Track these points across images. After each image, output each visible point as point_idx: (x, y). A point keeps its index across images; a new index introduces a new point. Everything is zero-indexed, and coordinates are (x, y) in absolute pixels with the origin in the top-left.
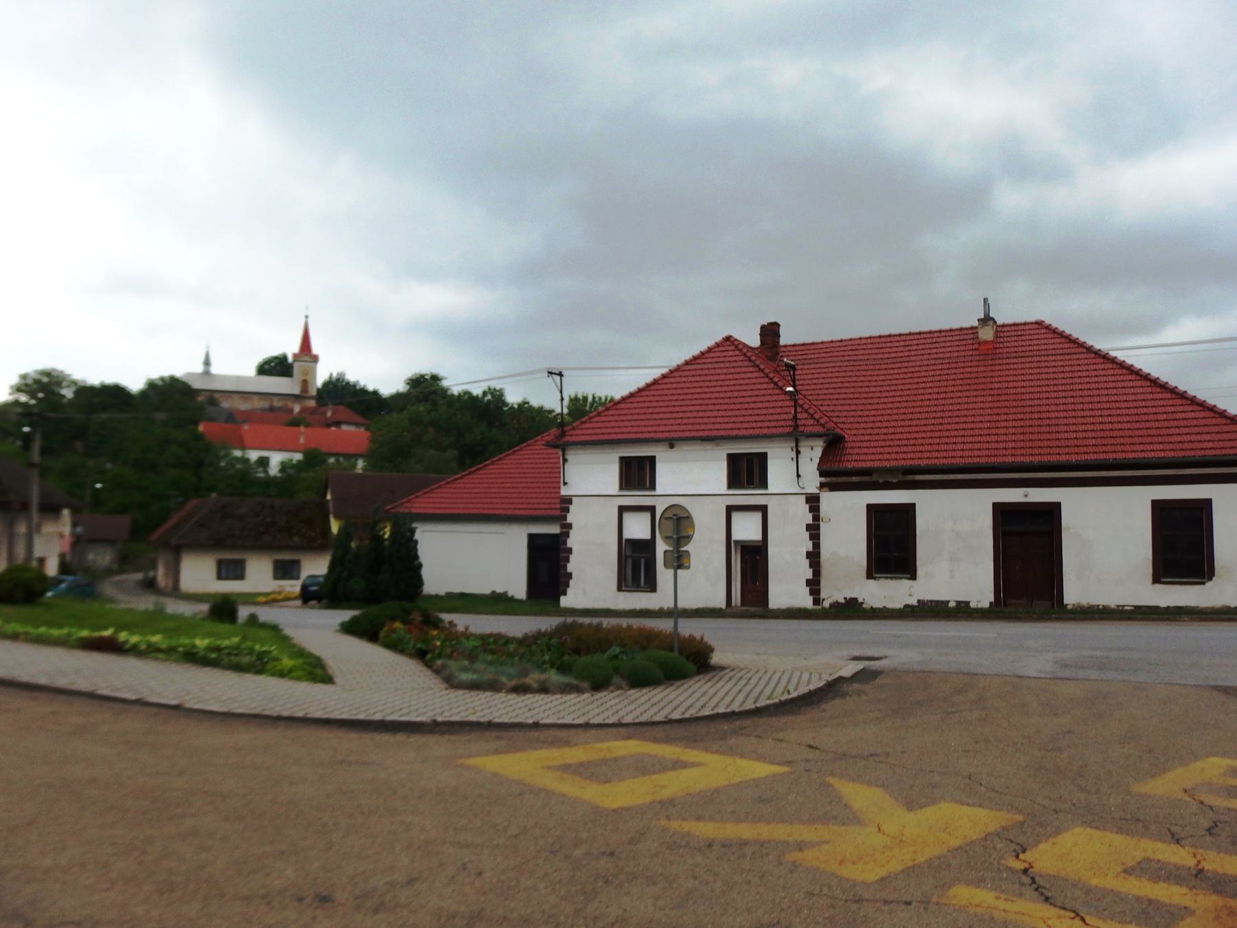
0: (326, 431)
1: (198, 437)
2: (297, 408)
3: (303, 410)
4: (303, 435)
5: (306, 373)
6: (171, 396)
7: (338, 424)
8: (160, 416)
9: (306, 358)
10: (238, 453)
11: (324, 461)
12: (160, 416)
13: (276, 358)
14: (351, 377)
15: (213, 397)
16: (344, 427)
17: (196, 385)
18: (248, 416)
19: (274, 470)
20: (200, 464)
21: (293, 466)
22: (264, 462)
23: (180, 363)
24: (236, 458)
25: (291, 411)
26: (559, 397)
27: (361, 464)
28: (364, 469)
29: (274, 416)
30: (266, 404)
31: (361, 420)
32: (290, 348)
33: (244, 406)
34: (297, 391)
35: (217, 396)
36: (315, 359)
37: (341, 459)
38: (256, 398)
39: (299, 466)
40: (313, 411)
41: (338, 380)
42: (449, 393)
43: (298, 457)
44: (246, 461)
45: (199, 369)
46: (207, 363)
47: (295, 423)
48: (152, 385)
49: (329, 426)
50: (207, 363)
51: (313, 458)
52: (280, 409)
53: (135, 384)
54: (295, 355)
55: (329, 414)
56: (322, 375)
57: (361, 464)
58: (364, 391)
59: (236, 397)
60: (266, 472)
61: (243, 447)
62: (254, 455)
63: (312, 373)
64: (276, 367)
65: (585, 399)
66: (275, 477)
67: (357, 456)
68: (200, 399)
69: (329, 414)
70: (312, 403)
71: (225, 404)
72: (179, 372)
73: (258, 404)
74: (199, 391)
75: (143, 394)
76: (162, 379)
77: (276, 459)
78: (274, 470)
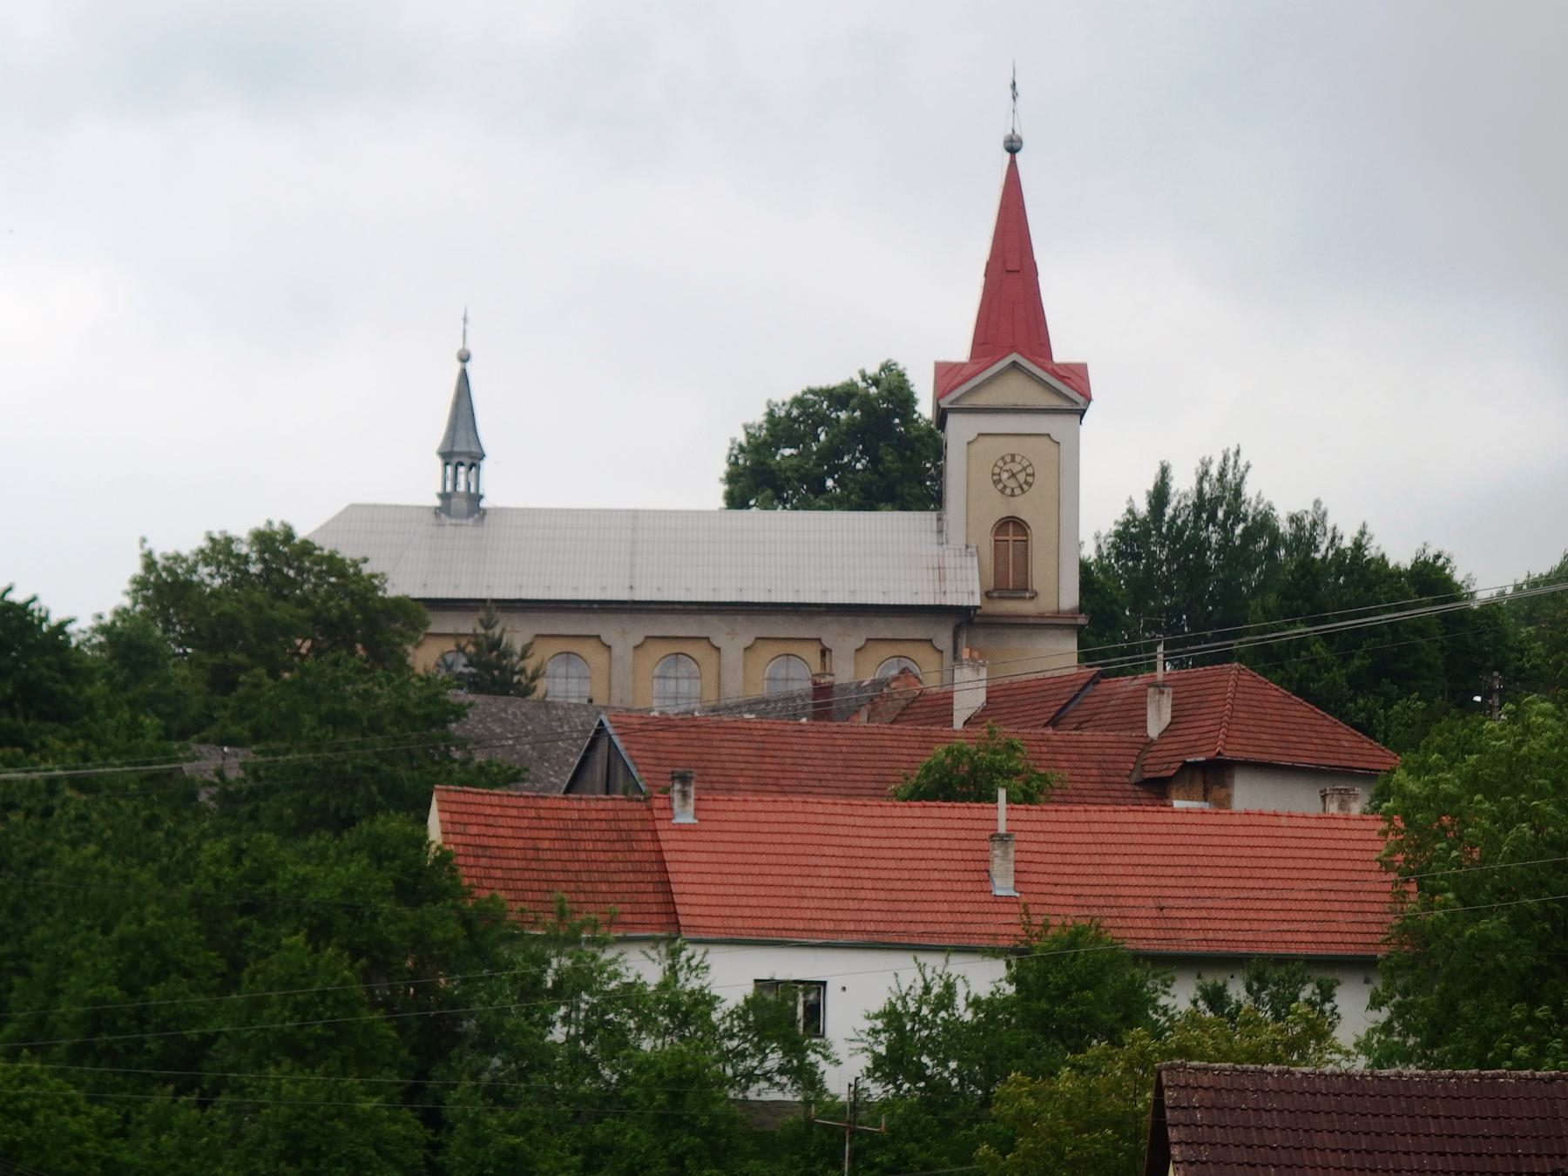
0: (1137, 819)
1: (421, 882)
2: (969, 697)
3: (1000, 700)
4: (1008, 853)
5: (1014, 477)
6: (270, 639)
7: (1212, 775)
8: (213, 764)
9: (1015, 390)
10: (642, 967)
11: (1134, 1007)
12: (213, 764)
13: (841, 397)
14: (1277, 491)
15: (495, 645)
16: (1248, 795)
17: (405, 579)
18: (699, 752)
19: (845, 1065)
20: (434, 1039)
21: (955, 1039)
22: (788, 1016)
23: (323, 463)
24: (631, 996)
25: (941, 707)
26: (469, 327)
27: (1355, 1015)
28: (1383, 1051)
29: (862, 734)
30: (796, 676)
31: (1348, 744)
32: (922, 328)
33: (661, 688)
34: (966, 590)
35: (516, 634)
36: (1070, 393)
37: (1237, 991)
38: (733, 639)
39: (991, 1040)
40: (1062, 707)
41: (1203, 506)
42: (1402, 567)
43: (983, 978)
44: (690, 1011)
45: (423, 483)
46: (462, 451)
47: (959, 783)
48: (164, 587)
49: (1157, 789)
50: (462, 451)
51: (1074, 991)
52: (875, 696)
53: (1489, 572)
54: (946, 375)
55: (1158, 719)
56: (1107, 483)
57: (1355, 1015)
58: (1360, 572)
59: (623, 636)
60: (808, 1078)
61: (668, 928)
62: (731, 977)
63: (1037, 476)
64: (845, 449)
65: (43, 619)
66: (858, 1102)
67: (1334, 966)
68: (424, 657)
69: (1158, 719)
70: (1058, 656)
71: (564, 684)
72: (307, 499)
73: (747, 673)
74: (415, 614)
75: (125, 642)
76: (220, 550)
77: (859, 993)
78: (845, 1065)
